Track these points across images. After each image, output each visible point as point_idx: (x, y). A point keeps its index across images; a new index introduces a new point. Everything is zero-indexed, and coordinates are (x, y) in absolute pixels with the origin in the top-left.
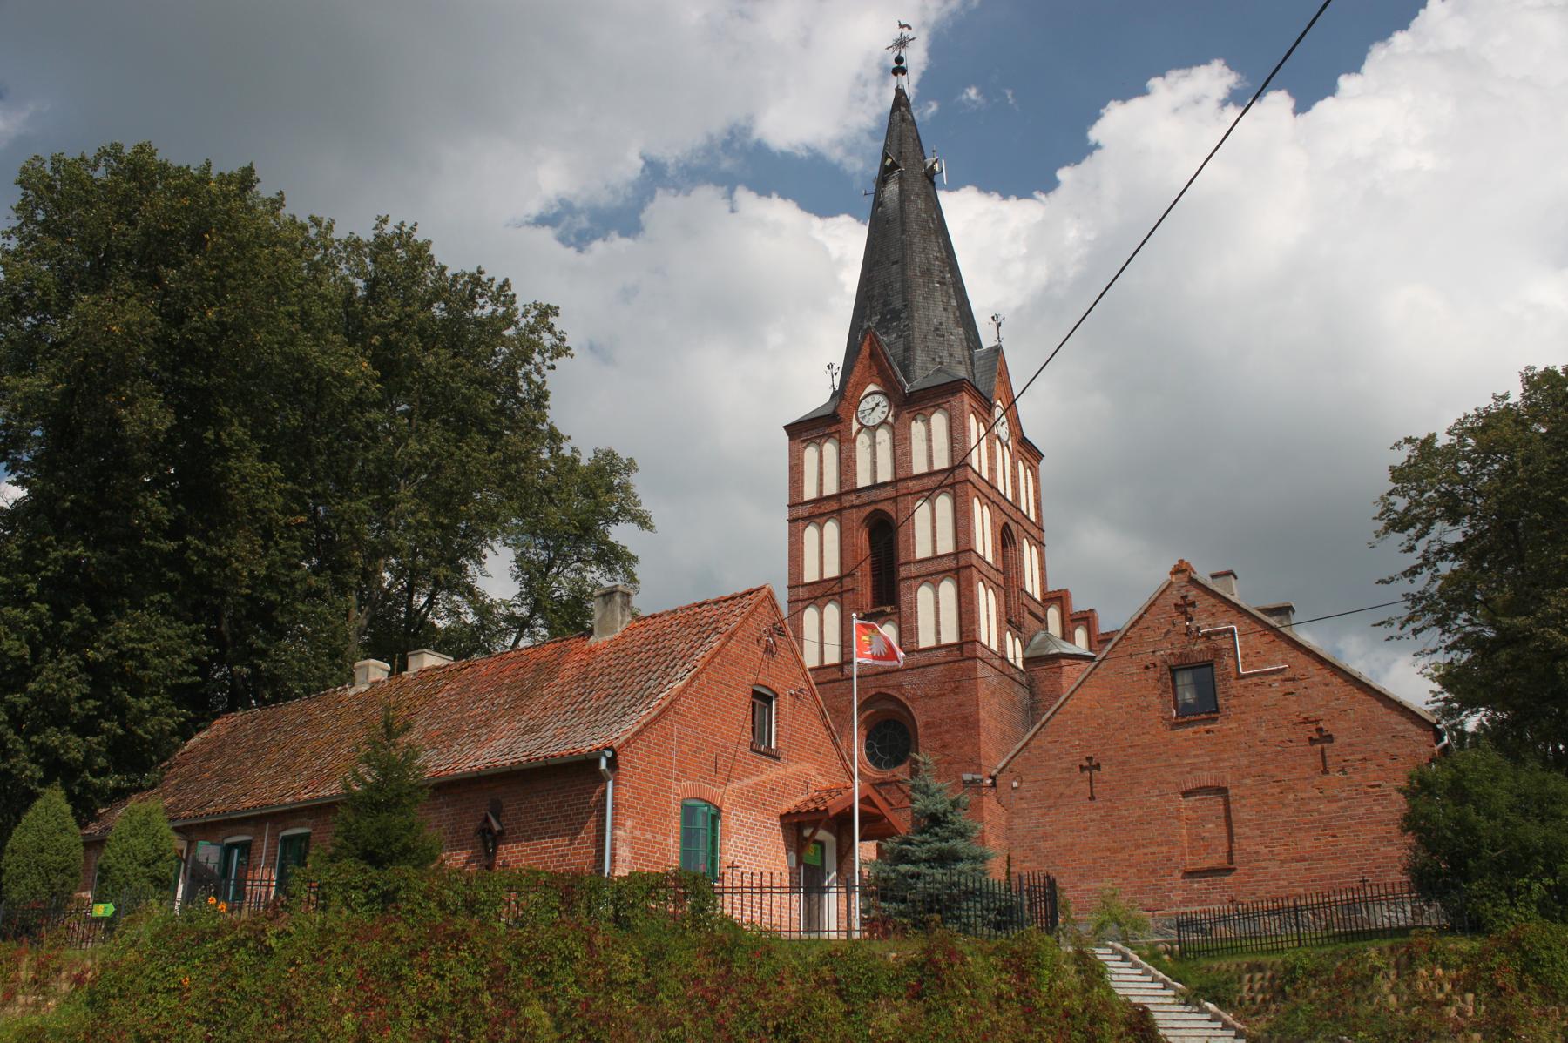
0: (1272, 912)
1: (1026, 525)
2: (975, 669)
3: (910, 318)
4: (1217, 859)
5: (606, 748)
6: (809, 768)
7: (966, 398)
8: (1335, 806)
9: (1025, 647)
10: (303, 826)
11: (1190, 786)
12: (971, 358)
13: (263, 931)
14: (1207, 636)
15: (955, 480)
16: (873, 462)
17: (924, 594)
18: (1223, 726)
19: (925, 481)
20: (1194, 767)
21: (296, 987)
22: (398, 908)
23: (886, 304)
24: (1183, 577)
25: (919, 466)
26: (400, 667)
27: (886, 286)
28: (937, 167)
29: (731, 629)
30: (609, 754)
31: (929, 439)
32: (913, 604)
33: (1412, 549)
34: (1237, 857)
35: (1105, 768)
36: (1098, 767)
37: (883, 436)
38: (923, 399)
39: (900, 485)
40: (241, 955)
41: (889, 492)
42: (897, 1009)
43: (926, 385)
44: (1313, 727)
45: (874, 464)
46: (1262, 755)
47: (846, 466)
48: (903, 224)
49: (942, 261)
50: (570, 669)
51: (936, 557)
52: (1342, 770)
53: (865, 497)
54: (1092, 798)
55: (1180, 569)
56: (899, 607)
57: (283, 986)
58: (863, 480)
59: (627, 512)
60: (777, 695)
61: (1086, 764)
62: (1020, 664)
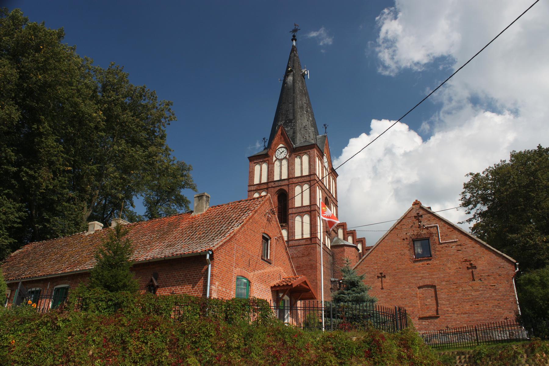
0: (454, 334)
1: (333, 199)
2: (316, 247)
3: (296, 122)
4: (432, 313)
5: (209, 250)
6: (280, 269)
7: (316, 151)
8: (478, 293)
9: (331, 242)
10: (65, 283)
11: (421, 284)
12: (316, 138)
13: (56, 319)
14: (427, 228)
15: (311, 180)
16: (280, 171)
17: (298, 219)
18: (434, 262)
19: (299, 179)
20: (423, 277)
21: (71, 346)
22: (122, 311)
23: (287, 117)
24: (418, 206)
25: (297, 174)
26: (106, 225)
27: (287, 111)
28: (306, 72)
29: (256, 208)
30: (211, 253)
31: (302, 165)
32: (293, 223)
33: (469, 213)
34: (440, 312)
35: (387, 277)
36: (385, 276)
37: (285, 162)
38: (300, 150)
39: (290, 180)
40: (44, 330)
41: (286, 182)
42: (361, 362)
43: (301, 145)
44: (468, 263)
45: (281, 172)
46: (449, 273)
47: (270, 173)
48: (294, 90)
49: (307, 104)
50: (184, 224)
51: (302, 207)
52: (480, 279)
53: (277, 184)
54: (382, 289)
55: (416, 203)
56: (288, 224)
57: (65, 345)
58: (277, 178)
59: (188, 184)
60: (270, 238)
61: (380, 275)
62: (329, 248)
